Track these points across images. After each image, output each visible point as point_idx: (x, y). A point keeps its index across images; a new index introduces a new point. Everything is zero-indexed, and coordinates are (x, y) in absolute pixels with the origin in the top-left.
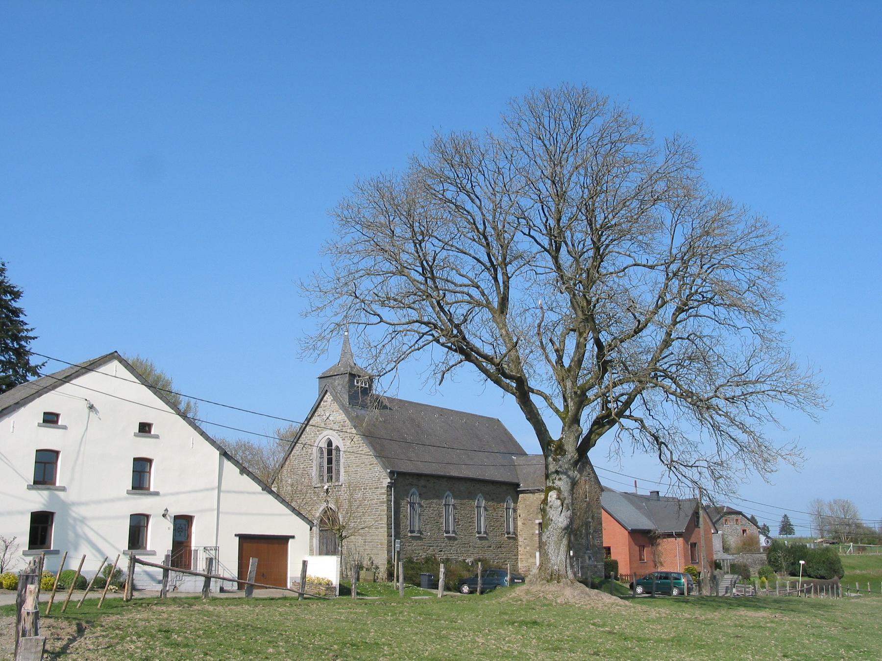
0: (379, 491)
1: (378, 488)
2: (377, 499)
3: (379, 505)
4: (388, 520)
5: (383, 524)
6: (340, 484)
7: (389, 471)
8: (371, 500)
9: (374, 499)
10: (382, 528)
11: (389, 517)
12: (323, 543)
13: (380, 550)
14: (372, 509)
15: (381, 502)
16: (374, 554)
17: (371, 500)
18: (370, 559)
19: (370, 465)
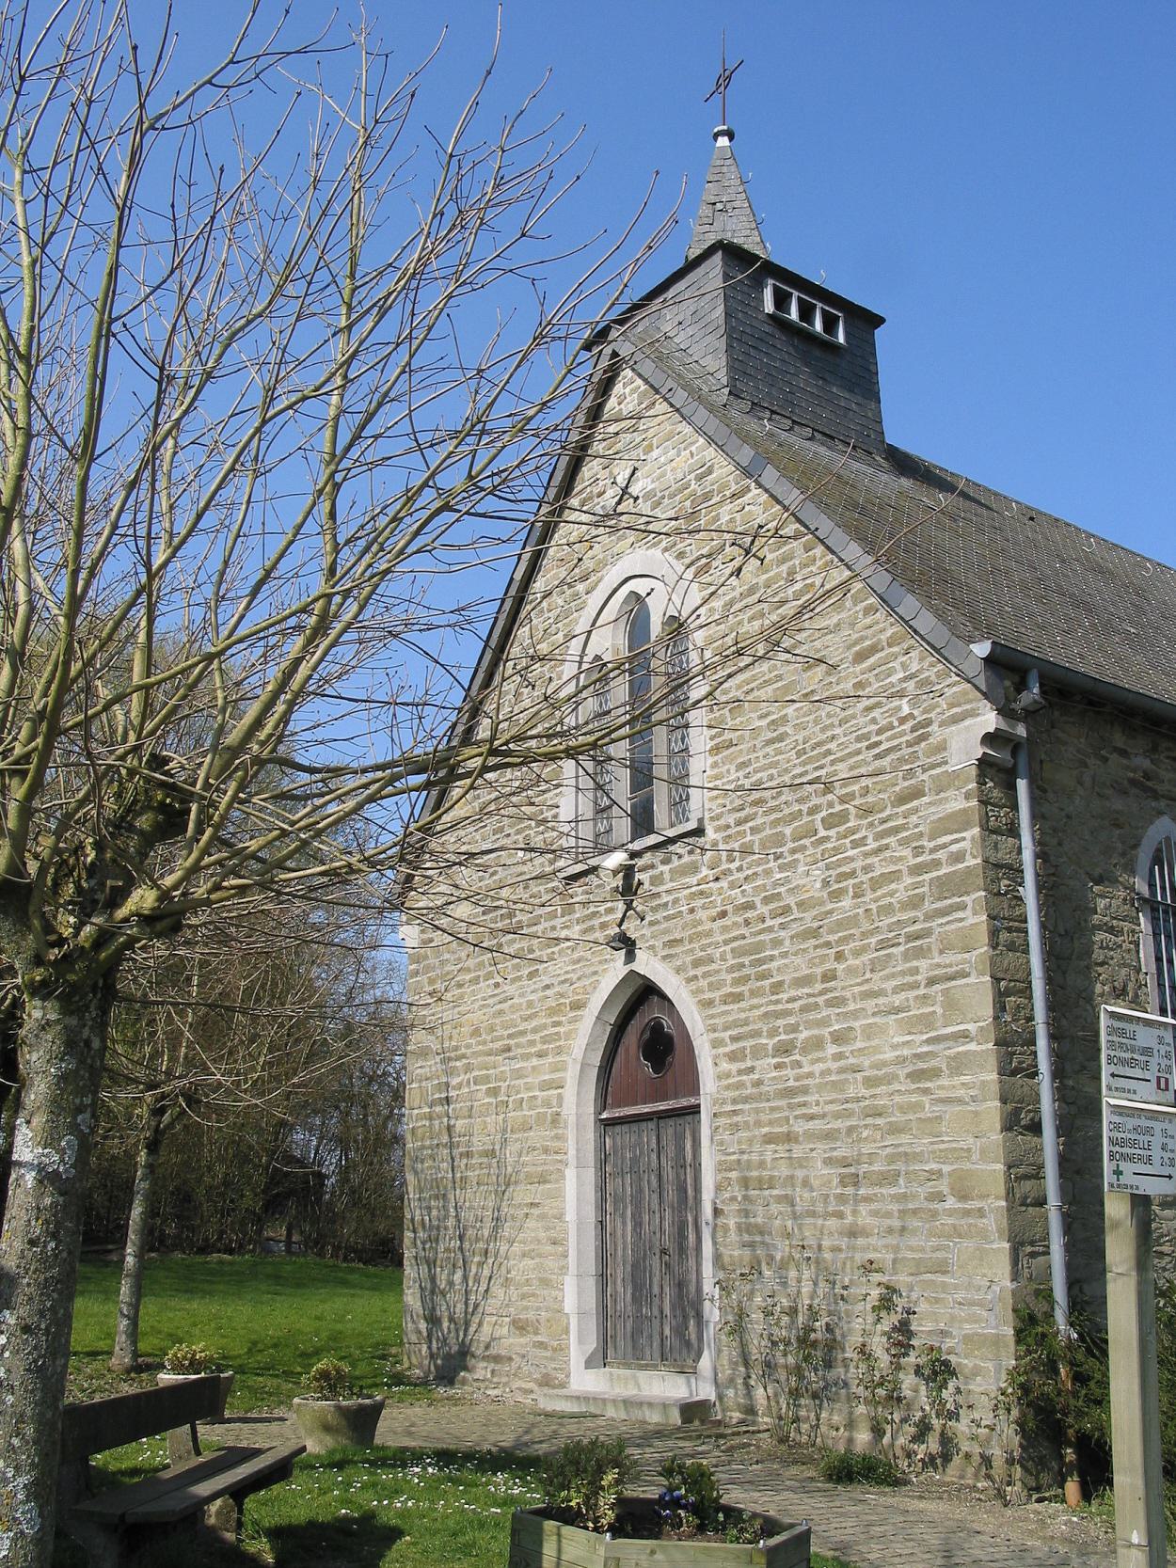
0: (930, 810)
1: (917, 793)
2: (917, 870)
3: (928, 906)
4: (1000, 1007)
5: (965, 1035)
6: (692, 825)
7: (982, 649)
8: (875, 883)
9: (894, 876)
10: (958, 1064)
11: (1008, 990)
12: (618, 1200)
13: (957, 1233)
14: (883, 945)
15: (946, 887)
16: (919, 1268)
17: (875, 883)
18: (886, 1304)
19: (860, 657)
